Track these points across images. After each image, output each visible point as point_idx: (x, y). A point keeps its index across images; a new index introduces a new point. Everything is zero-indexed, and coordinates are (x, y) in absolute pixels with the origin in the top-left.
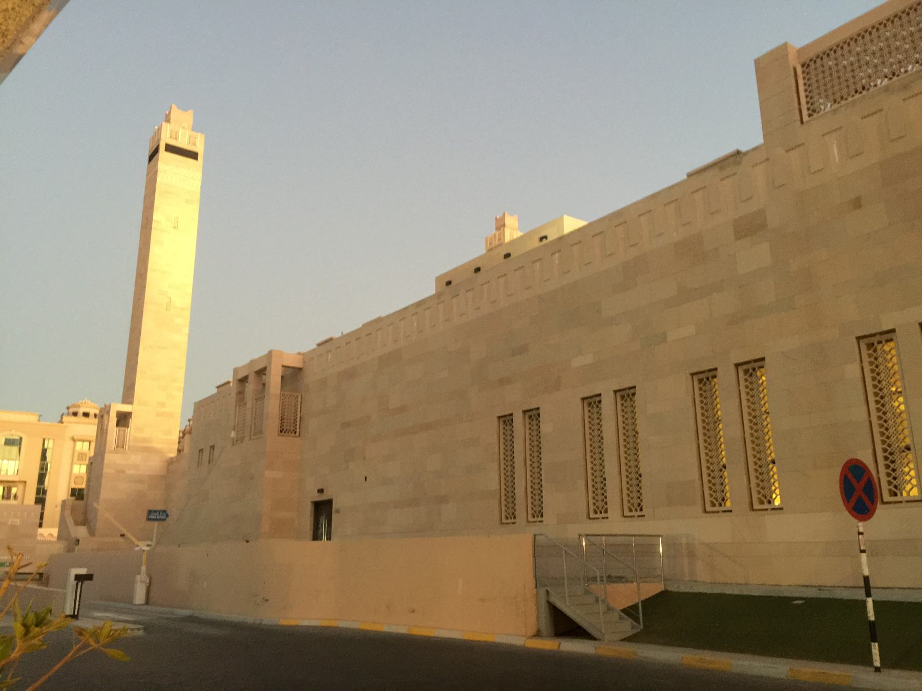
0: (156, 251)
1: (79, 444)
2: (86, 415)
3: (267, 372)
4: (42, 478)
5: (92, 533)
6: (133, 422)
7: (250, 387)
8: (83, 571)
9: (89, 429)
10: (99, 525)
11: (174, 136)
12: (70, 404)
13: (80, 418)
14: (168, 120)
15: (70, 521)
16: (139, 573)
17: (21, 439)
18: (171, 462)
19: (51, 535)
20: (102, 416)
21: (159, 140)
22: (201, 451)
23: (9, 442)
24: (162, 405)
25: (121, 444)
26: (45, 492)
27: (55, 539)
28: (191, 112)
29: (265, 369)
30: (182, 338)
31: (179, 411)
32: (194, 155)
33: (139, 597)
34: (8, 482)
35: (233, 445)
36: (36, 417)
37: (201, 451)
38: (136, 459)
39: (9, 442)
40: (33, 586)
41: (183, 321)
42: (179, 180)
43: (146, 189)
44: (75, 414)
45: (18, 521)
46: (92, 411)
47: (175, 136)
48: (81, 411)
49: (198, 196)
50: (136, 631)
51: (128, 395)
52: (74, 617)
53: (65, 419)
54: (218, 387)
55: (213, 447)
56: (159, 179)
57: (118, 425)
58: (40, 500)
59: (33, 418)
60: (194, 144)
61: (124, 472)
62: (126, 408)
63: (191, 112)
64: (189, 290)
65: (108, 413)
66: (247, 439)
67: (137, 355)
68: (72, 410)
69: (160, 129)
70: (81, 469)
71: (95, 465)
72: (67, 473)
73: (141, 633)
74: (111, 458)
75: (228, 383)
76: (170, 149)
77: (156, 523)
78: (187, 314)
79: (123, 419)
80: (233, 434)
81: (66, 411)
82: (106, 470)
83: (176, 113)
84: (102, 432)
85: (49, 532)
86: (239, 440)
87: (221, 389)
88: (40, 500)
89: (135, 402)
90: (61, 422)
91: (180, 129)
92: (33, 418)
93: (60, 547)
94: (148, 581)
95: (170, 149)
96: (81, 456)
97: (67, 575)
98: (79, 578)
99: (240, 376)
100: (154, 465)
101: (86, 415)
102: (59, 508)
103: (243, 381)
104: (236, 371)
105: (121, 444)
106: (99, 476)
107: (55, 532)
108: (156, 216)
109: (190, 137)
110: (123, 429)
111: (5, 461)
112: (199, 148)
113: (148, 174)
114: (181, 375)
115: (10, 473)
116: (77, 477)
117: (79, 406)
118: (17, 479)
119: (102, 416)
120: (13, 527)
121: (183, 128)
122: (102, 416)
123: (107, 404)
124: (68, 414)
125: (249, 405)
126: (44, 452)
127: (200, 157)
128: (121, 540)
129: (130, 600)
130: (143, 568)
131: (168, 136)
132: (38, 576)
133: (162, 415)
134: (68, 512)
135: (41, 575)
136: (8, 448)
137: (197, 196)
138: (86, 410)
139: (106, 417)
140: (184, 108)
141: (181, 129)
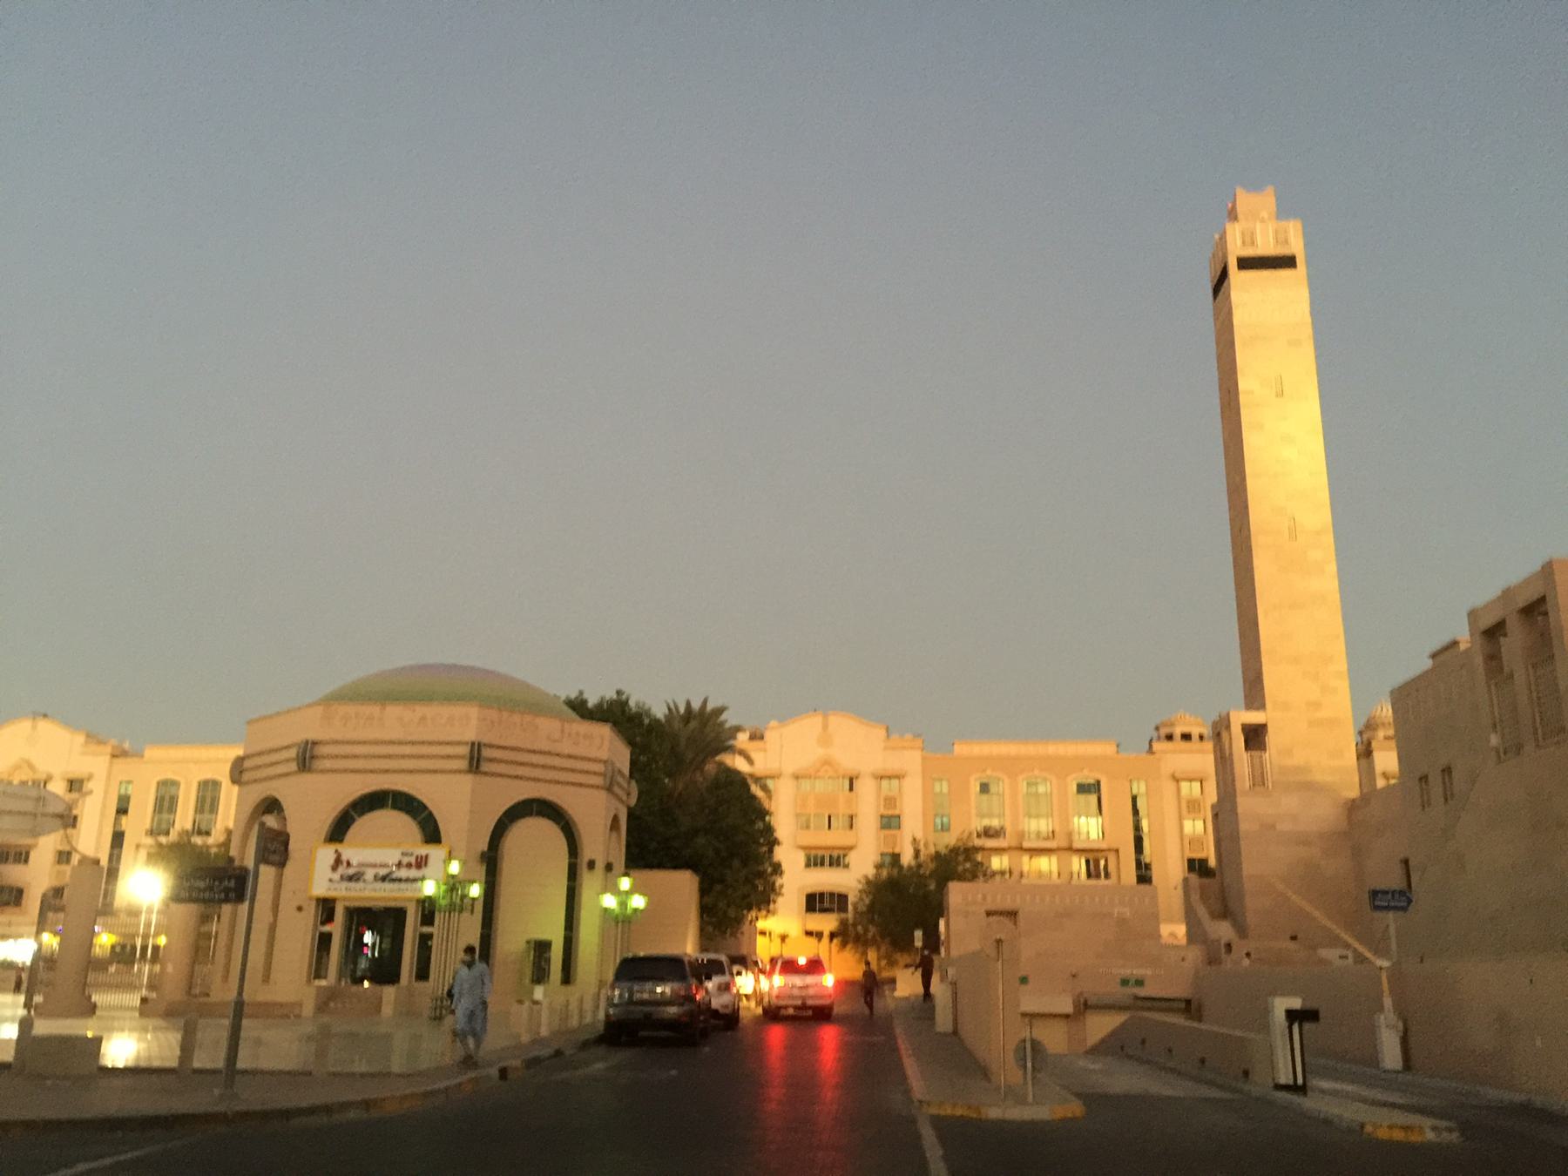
0: (1252, 441)
1: (1184, 785)
2: (1186, 737)
3: (1549, 605)
4: (1139, 841)
5: (1242, 931)
6: (1272, 739)
7: (1514, 644)
8: (1296, 1003)
9: (1202, 760)
10: (1251, 920)
11: (1248, 239)
12: (1158, 721)
13: (1178, 744)
14: (1233, 215)
15: (1202, 912)
16: (1381, 1009)
17: (1098, 782)
18: (1352, 807)
19: (1172, 935)
20: (1220, 730)
21: (1225, 256)
22: (1424, 779)
23: (1083, 789)
24: (1317, 705)
25: (1259, 779)
26: (1148, 867)
27: (1184, 941)
28: (1270, 190)
29: (1542, 600)
30: (1327, 582)
31: (1350, 714)
32: (1288, 262)
33: (1391, 1056)
34: (1092, 850)
35: (1499, 761)
36: (1114, 748)
37: (1424, 779)
38: (1290, 803)
39: (1083, 789)
40: (1178, 1020)
41: (1324, 554)
42: (1272, 312)
43: (1218, 344)
44: (1170, 737)
45: (1127, 912)
46: (1195, 731)
47: (1249, 239)
48: (1178, 731)
49: (1308, 331)
50: (1445, 1134)
51: (1254, 693)
52: (1301, 1090)
53: (1156, 746)
54: (1434, 656)
55: (1447, 771)
56: (1236, 322)
57: (1247, 747)
58: (1144, 875)
59: (1110, 749)
60: (1286, 242)
61: (1273, 827)
62: (1255, 717)
63: (1270, 190)
64: (1324, 495)
65: (1228, 727)
66: (1529, 748)
67: (1256, 625)
68: (1164, 731)
69: (1223, 237)
70: (1196, 826)
71: (1224, 815)
72: (1182, 832)
73: (1454, 1137)
74: (1248, 805)
75: (1455, 643)
76: (1246, 263)
77: (1391, 915)
78: (1329, 539)
79: (1255, 736)
80: (1494, 740)
81: (1155, 735)
82: (1244, 826)
83: (1245, 201)
84: (1224, 761)
85: (1174, 931)
86: (1503, 754)
87: (1441, 658)
88: (1144, 875)
89: (1269, 705)
90: (1150, 751)
91: (1259, 225)
92: (1110, 749)
93: (1195, 955)
94: (1400, 1025)
95: (1246, 263)
96: (1193, 806)
97: (1267, 1011)
98: (1292, 1015)
99: (1488, 621)
100: (1321, 814)
101: (1186, 737)
102: (1180, 891)
103: (1493, 633)
104: (1473, 615)
105: (1259, 779)
106: (1235, 838)
107: (1181, 930)
108: (1243, 384)
109: (1276, 232)
110: (1256, 754)
111: (1083, 819)
112: (1296, 247)
113: (1216, 319)
114: (1340, 647)
115: (1094, 835)
116: (1195, 841)
117: (1172, 725)
118: (1104, 846)
119: (1218, 735)
120: (1122, 922)
121: (1263, 221)
122: (1220, 730)
123: (1224, 714)
124: (1159, 738)
125: (1520, 677)
126: (1134, 799)
127: (1300, 261)
128: (1292, 945)
129: (1373, 1060)
130: (1388, 1002)
131: (1239, 242)
132: (1183, 1005)
133: (1324, 716)
134: (1195, 897)
135: (1188, 1002)
136: (1082, 797)
137: (1307, 331)
138: (1186, 730)
139: (1224, 735)
140: (1255, 187)
141: (1259, 226)
